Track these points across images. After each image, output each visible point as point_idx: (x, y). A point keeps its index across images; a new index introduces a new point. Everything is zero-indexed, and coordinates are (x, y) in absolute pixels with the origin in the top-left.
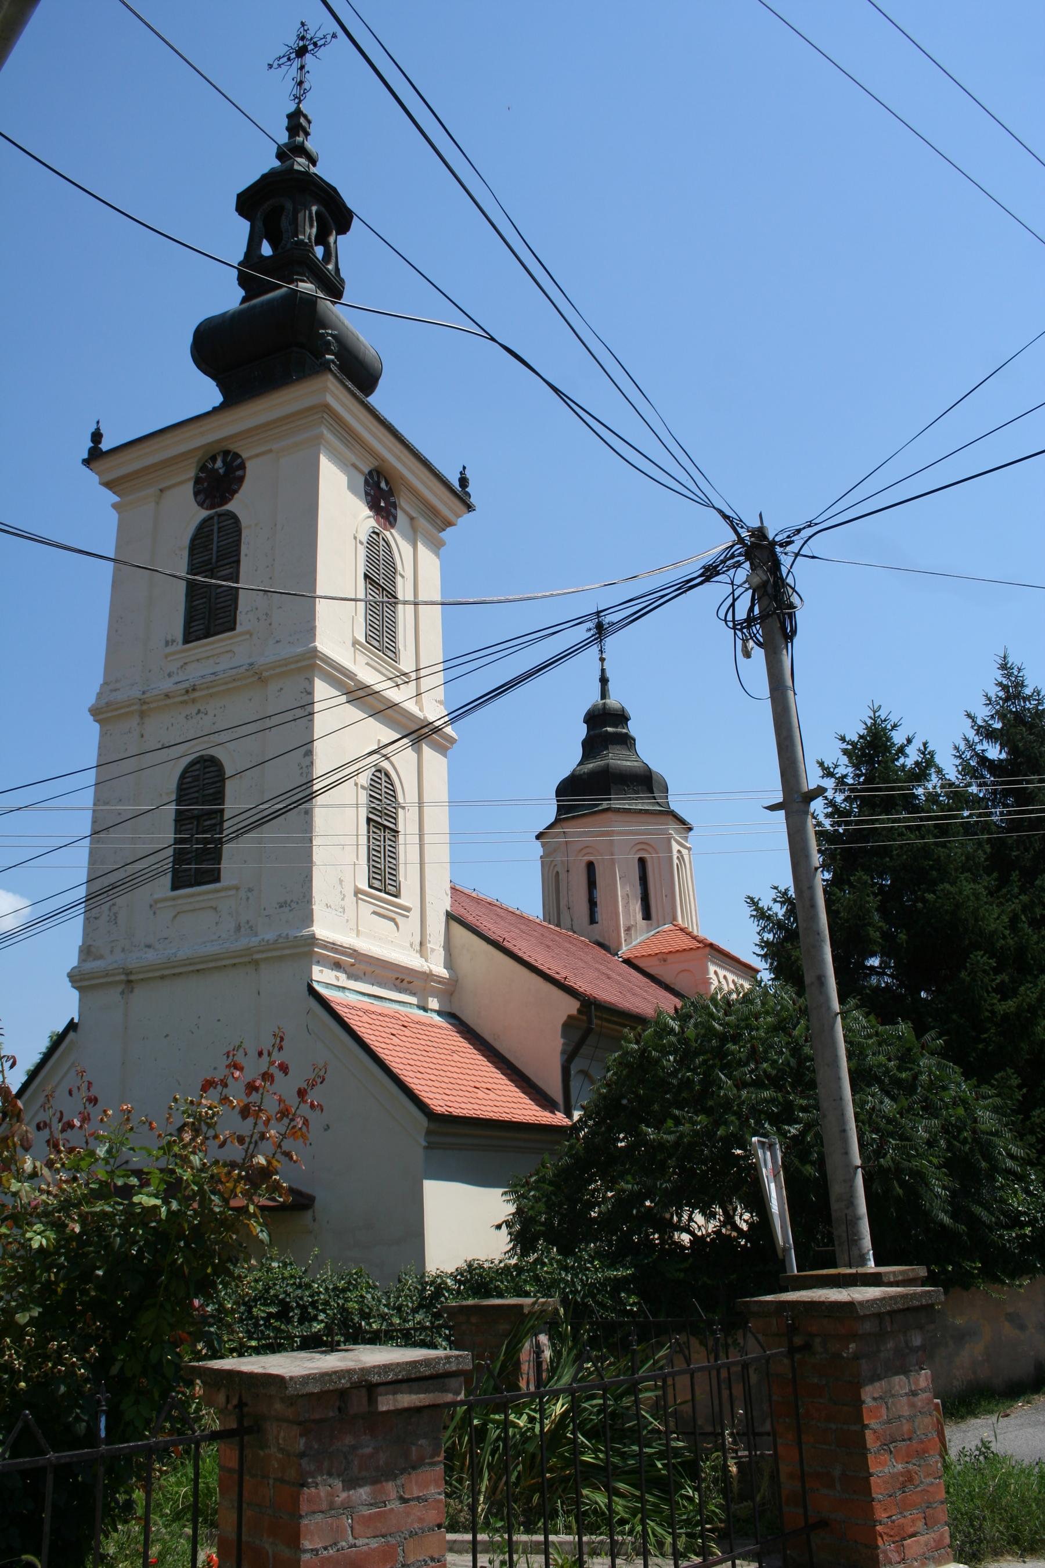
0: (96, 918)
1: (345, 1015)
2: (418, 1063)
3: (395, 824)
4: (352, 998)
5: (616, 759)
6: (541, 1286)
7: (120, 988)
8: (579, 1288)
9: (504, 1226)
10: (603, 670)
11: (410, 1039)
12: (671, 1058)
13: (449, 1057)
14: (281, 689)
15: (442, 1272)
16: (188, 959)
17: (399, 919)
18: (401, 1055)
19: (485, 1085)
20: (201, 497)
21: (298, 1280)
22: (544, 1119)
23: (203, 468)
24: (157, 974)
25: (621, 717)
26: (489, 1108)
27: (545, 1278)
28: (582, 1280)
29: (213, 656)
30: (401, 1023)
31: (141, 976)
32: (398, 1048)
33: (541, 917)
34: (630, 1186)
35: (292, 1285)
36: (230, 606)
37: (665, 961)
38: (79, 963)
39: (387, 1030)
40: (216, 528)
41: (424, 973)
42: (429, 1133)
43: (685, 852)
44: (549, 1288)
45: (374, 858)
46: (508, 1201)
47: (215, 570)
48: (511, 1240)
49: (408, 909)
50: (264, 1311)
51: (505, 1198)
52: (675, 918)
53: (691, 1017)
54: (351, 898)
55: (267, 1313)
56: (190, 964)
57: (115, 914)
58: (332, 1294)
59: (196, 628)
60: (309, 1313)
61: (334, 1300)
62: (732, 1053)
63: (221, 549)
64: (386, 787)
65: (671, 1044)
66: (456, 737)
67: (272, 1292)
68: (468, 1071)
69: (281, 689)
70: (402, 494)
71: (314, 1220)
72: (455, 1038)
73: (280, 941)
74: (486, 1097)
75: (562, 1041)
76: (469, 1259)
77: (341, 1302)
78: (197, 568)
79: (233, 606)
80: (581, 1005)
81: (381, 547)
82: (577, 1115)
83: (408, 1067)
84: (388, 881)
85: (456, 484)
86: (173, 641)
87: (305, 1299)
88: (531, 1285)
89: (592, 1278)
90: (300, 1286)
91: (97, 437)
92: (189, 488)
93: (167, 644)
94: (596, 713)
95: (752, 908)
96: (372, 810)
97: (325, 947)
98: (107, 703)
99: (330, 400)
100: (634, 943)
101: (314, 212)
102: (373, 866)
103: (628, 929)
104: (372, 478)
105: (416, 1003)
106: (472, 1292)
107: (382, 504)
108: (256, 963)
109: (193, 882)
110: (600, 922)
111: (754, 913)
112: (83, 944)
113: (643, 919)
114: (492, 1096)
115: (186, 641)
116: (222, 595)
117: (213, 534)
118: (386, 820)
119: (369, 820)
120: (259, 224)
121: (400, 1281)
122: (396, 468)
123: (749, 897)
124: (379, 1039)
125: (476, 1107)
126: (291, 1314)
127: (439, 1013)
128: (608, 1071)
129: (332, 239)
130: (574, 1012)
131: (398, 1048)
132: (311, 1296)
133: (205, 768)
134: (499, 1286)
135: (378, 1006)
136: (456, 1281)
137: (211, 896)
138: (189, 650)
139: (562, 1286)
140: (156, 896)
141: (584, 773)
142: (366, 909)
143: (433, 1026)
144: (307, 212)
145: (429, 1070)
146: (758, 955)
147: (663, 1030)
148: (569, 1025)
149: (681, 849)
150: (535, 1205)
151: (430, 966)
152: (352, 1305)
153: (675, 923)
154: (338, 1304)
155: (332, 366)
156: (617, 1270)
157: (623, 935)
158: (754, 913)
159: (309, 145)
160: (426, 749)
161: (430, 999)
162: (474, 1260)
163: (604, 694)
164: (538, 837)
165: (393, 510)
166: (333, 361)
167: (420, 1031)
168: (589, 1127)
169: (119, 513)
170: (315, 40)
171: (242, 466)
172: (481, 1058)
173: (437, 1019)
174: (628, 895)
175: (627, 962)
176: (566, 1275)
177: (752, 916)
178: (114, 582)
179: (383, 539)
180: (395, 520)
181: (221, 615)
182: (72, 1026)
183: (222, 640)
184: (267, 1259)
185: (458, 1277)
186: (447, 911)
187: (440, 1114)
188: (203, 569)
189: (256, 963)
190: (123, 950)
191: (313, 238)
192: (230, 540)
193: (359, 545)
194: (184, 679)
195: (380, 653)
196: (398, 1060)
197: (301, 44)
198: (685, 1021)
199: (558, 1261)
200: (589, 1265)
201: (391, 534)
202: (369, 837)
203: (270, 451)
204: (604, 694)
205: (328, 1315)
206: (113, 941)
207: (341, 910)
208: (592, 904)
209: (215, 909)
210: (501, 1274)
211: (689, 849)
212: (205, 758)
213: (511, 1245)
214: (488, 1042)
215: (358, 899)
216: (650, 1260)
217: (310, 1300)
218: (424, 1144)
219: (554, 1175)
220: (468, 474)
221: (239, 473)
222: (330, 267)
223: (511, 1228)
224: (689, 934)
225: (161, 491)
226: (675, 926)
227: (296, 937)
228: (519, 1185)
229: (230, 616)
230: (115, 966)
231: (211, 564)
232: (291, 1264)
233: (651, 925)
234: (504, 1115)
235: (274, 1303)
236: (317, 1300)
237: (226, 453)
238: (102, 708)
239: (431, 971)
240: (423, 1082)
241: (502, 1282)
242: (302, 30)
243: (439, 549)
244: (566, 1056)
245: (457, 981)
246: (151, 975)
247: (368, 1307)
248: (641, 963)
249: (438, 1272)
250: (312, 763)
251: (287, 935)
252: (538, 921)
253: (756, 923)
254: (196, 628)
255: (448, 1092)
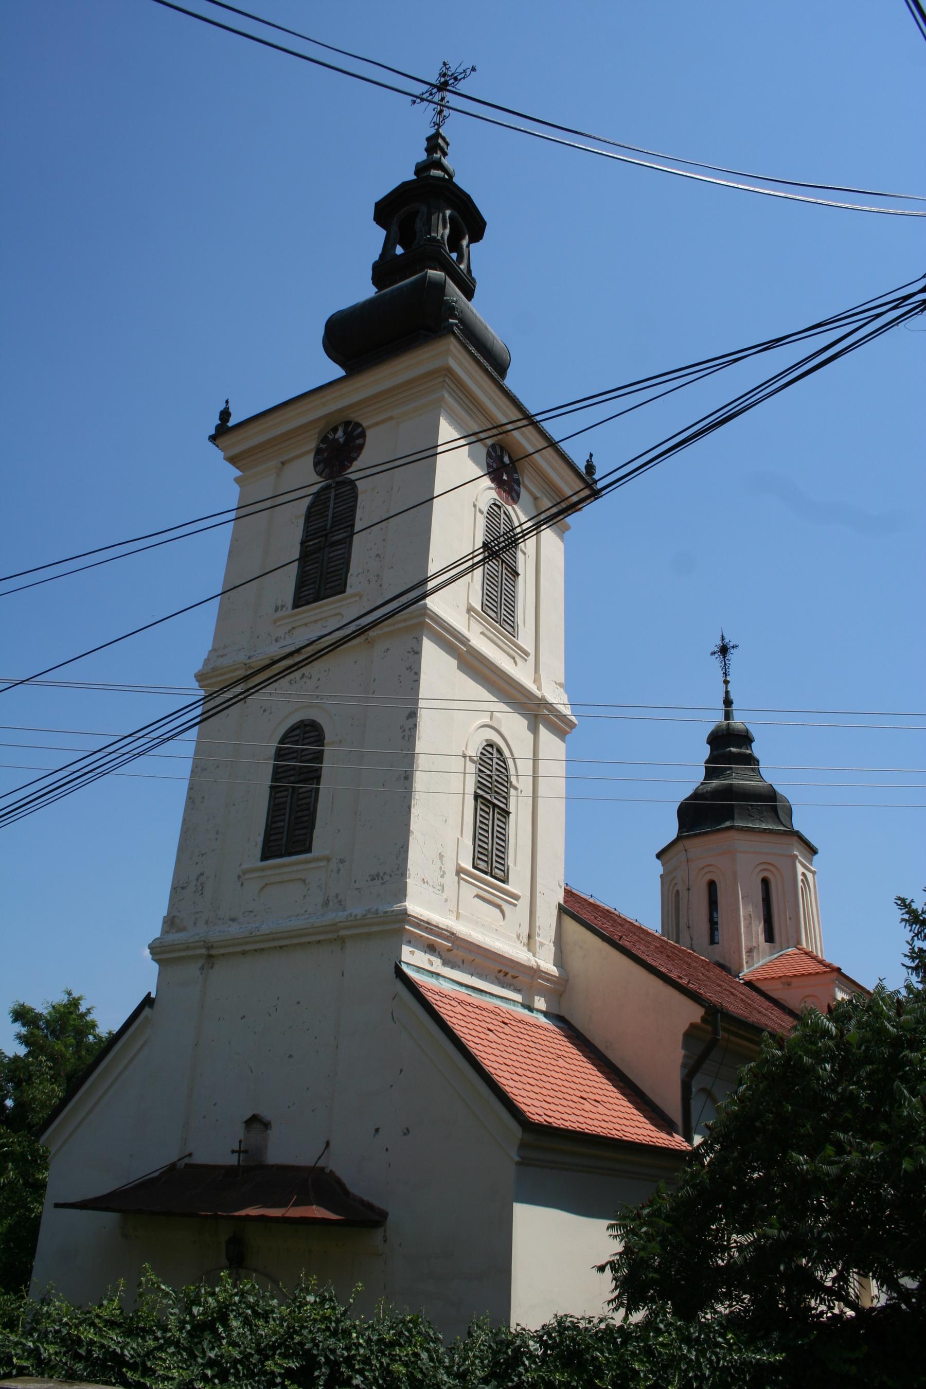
0: (183, 888)
1: (434, 1002)
2: (516, 1064)
3: (506, 805)
4: (446, 987)
5: (739, 779)
6: (655, 1364)
7: (201, 962)
8: (707, 1373)
9: (608, 1269)
10: (727, 693)
11: (509, 1037)
12: (828, 1067)
13: (553, 1062)
14: (388, 649)
15: (523, 1329)
16: (271, 933)
17: (506, 907)
18: (497, 1052)
19: (593, 1097)
20: (321, 467)
21: (333, 1324)
22: (660, 1141)
23: (324, 440)
24: (239, 949)
25: (745, 739)
26: (596, 1123)
27: (660, 1353)
28: (710, 1361)
29: (321, 619)
30: (500, 1019)
31: (222, 951)
32: (494, 1045)
33: (660, 931)
34: (776, 1232)
35: (324, 1330)
36: (342, 569)
37: (789, 984)
38: (161, 935)
39: (483, 1024)
40: (332, 495)
41: (531, 968)
42: (523, 1146)
43: (809, 875)
44: (665, 1368)
45: (481, 837)
46: (615, 1237)
47: (329, 535)
48: (616, 1288)
49: (516, 897)
50: (281, 1366)
51: (610, 1232)
52: (799, 942)
53: (850, 1018)
54: (451, 877)
55: (286, 1369)
56: (273, 940)
57: (202, 884)
58: (375, 1348)
59: (306, 593)
60: (342, 1373)
61: (377, 1357)
62: (910, 1062)
63: (336, 515)
64: (497, 764)
65: (828, 1049)
66: (576, 722)
67: (297, 1339)
68: (575, 1079)
69: (388, 649)
70: (526, 471)
71: (385, 1241)
72: (562, 1043)
73: (369, 916)
74: (594, 1109)
75: (682, 1052)
76: (561, 1313)
77: (385, 1361)
78: (311, 535)
79: (344, 570)
80: (705, 1013)
81: (502, 521)
82: (698, 1140)
83: (504, 1067)
84: (495, 864)
85: (583, 470)
86: (283, 606)
87: (338, 1352)
88: (641, 1362)
89: (724, 1358)
90: (334, 1334)
91: (225, 415)
92: (310, 459)
93: (277, 609)
94: (720, 734)
95: (904, 911)
96: (480, 785)
97: (417, 926)
98: (212, 669)
99: (452, 363)
100: (756, 966)
101: (447, 215)
102: (479, 846)
103: (750, 951)
104: (496, 452)
105: (521, 1001)
106: (562, 1364)
107: (505, 477)
108: (342, 940)
109: (283, 853)
110: (720, 942)
111: (906, 917)
112: (168, 915)
113: (766, 941)
114: (601, 1109)
115: (296, 606)
116: (334, 559)
117: (329, 501)
118: (495, 798)
119: (477, 797)
120: (395, 228)
121: (470, 1335)
122: (519, 443)
123: (899, 899)
124: (473, 1033)
125: (581, 1119)
126: (316, 1373)
127: (546, 1014)
128: (741, 1085)
129: (465, 242)
130: (698, 1020)
131: (494, 1045)
132: (348, 1348)
133: (305, 733)
134: (596, 1358)
135: (476, 998)
136: (543, 1344)
137: (301, 867)
138: (298, 614)
139: (683, 1367)
140: (245, 866)
141: (707, 791)
142: (469, 892)
143: (538, 1027)
144: (441, 215)
145: (528, 1073)
146: (908, 967)
147: (815, 1031)
148: (691, 1035)
149: (806, 872)
150: (648, 1244)
151: (539, 961)
152: (399, 1368)
153: (799, 946)
154: (381, 1364)
155: (455, 328)
156: (758, 1350)
157: (744, 957)
158: (906, 917)
159: (445, 161)
160: (543, 730)
161: (537, 998)
162: (566, 1315)
163: (728, 716)
164: (659, 856)
165: (516, 487)
166: (456, 325)
167: (523, 1031)
168: (716, 1152)
169: (240, 487)
170: (455, 75)
171: (363, 435)
172: (590, 1066)
173: (543, 1020)
174: (750, 915)
175: (749, 984)
176: (689, 1351)
177: (903, 920)
178: (230, 552)
179: (505, 513)
180: (518, 495)
181: (331, 579)
182: (148, 1001)
183: (333, 603)
184: (301, 1290)
185: (545, 1338)
186: (559, 904)
187: (535, 1124)
188: (318, 535)
189: (342, 940)
190: (207, 922)
191: (446, 238)
192: (345, 506)
193: (478, 513)
194: (291, 642)
195: (498, 625)
196: (492, 1058)
197: (443, 80)
198: (843, 1022)
199: (678, 1329)
200: (720, 1339)
201: (513, 509)
202: (476, 809)
203: (391, 418)
204: (728, 716)
205: (366, 1378)
206: (197, 912)
207: (440, 888)
208: (713, 925)
209: (304, 881)
210: (601, 1339)
211: (814, 873)
212: (306, 723)
213: (617, 1293)
214: (600, 1052)
215: (460, 879)
216: (806, 1341)
217: (346, 1354)
218: (517, 1159)
219: (672, 1209)
220: (595, 461)
221: (360, 441)
222: (462, 266)
223: (616, 1271)
224: (815, 958)
225: (283, 463)
226: (800, 949)
227: (386, 912)
228: (628, 1217)
229: (341, 579)
230: (197, 938)
231: (326, 530)
232: (331, 1300)
233: (774, 947)
234: (614, 1132)
235: (298, 1354)
236: (354, 1356)
237: (347, 423)
238: (207, 673)
239: (538, 966)
240: (519, 1085)
241: (602, 1352)
242: (444, 69)
243: (564, 533)
244: (686, 1071)
245: (567, 981)
246: (231, 950)
247: (421, 1371)
248: (763, 986)
249: (519, 1328)
250: (415, 725)
251: (377, 910)
252: (656, 934)
253: (908, 928)
254: (306, 593)
255: (549, 1099)
